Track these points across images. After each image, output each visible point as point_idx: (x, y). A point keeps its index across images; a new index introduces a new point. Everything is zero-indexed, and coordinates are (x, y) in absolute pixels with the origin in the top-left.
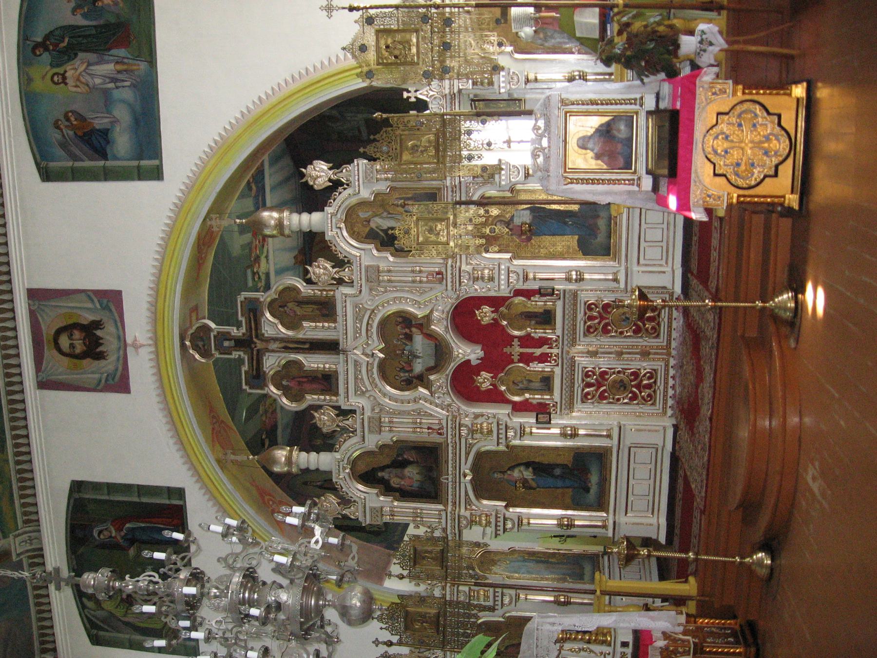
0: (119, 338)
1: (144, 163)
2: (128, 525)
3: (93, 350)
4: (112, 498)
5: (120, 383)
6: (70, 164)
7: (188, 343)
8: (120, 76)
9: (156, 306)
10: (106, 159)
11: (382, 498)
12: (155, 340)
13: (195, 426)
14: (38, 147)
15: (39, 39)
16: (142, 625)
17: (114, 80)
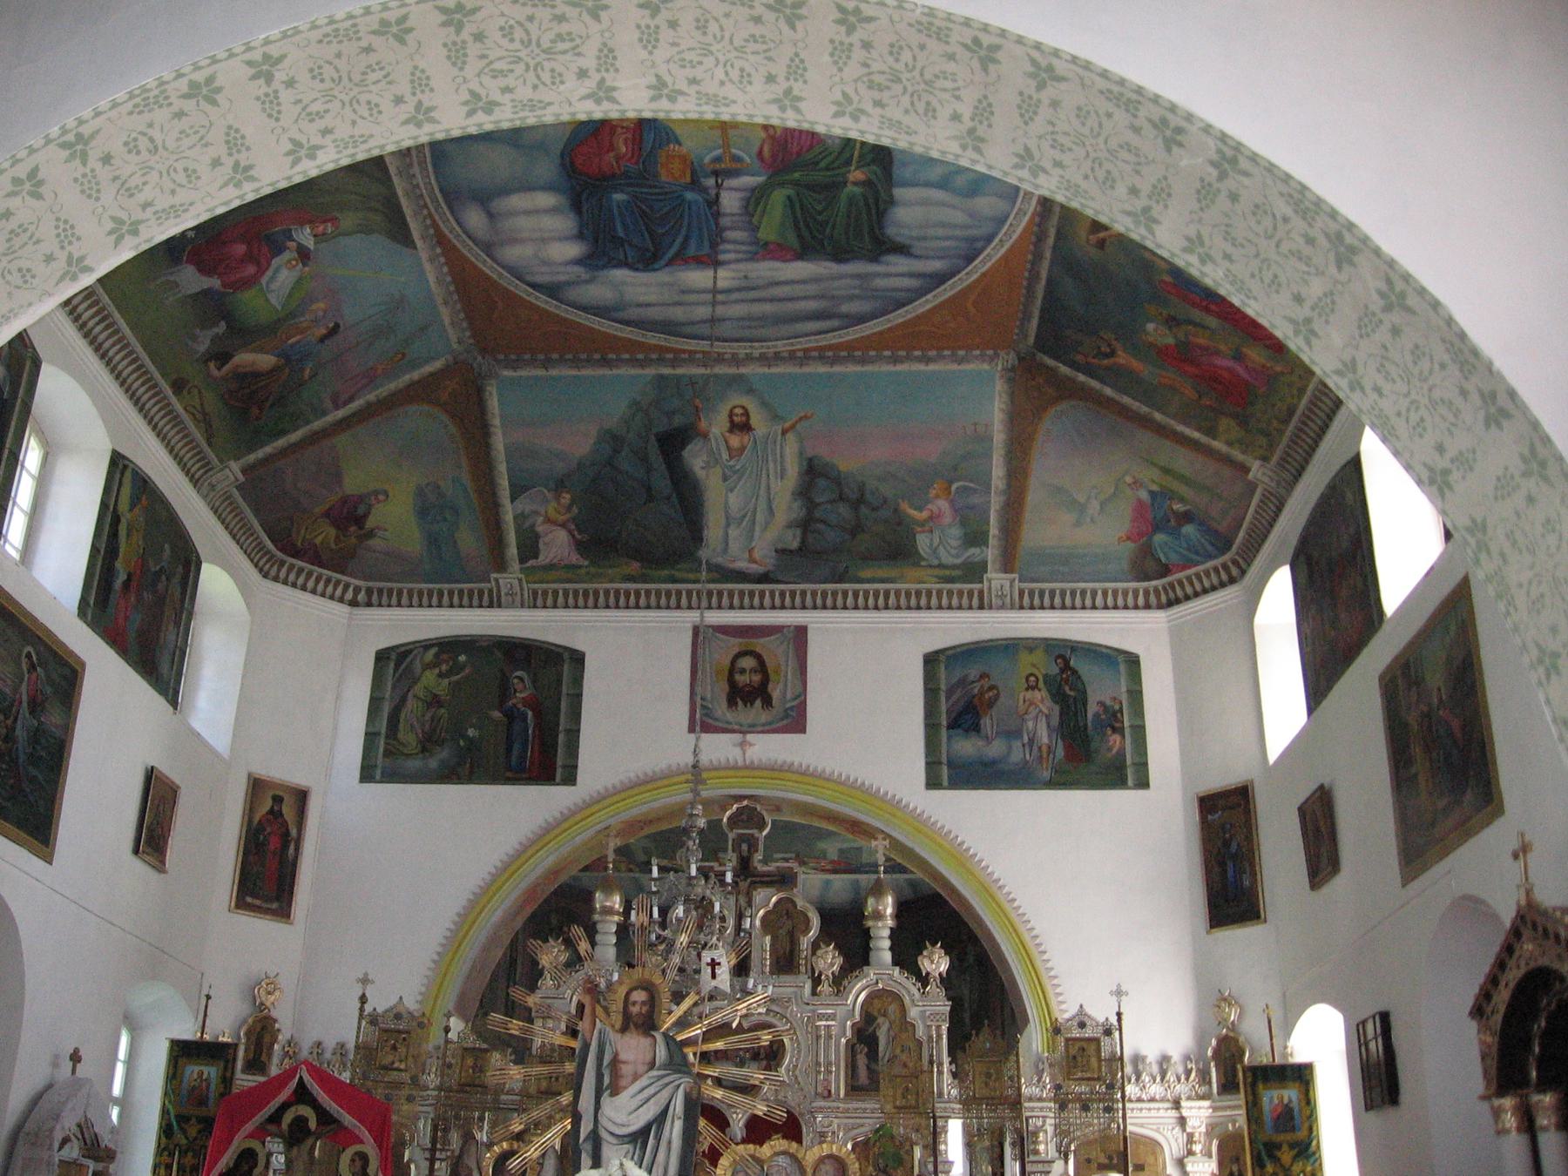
0: (753, 726)
2: (530, 713)
5: (702, 722)
6: (943, 687)
7: (745, 803)
8: (1035, 748)
12: (751, 767)
16: (403, 716)
17: (1031, 741)
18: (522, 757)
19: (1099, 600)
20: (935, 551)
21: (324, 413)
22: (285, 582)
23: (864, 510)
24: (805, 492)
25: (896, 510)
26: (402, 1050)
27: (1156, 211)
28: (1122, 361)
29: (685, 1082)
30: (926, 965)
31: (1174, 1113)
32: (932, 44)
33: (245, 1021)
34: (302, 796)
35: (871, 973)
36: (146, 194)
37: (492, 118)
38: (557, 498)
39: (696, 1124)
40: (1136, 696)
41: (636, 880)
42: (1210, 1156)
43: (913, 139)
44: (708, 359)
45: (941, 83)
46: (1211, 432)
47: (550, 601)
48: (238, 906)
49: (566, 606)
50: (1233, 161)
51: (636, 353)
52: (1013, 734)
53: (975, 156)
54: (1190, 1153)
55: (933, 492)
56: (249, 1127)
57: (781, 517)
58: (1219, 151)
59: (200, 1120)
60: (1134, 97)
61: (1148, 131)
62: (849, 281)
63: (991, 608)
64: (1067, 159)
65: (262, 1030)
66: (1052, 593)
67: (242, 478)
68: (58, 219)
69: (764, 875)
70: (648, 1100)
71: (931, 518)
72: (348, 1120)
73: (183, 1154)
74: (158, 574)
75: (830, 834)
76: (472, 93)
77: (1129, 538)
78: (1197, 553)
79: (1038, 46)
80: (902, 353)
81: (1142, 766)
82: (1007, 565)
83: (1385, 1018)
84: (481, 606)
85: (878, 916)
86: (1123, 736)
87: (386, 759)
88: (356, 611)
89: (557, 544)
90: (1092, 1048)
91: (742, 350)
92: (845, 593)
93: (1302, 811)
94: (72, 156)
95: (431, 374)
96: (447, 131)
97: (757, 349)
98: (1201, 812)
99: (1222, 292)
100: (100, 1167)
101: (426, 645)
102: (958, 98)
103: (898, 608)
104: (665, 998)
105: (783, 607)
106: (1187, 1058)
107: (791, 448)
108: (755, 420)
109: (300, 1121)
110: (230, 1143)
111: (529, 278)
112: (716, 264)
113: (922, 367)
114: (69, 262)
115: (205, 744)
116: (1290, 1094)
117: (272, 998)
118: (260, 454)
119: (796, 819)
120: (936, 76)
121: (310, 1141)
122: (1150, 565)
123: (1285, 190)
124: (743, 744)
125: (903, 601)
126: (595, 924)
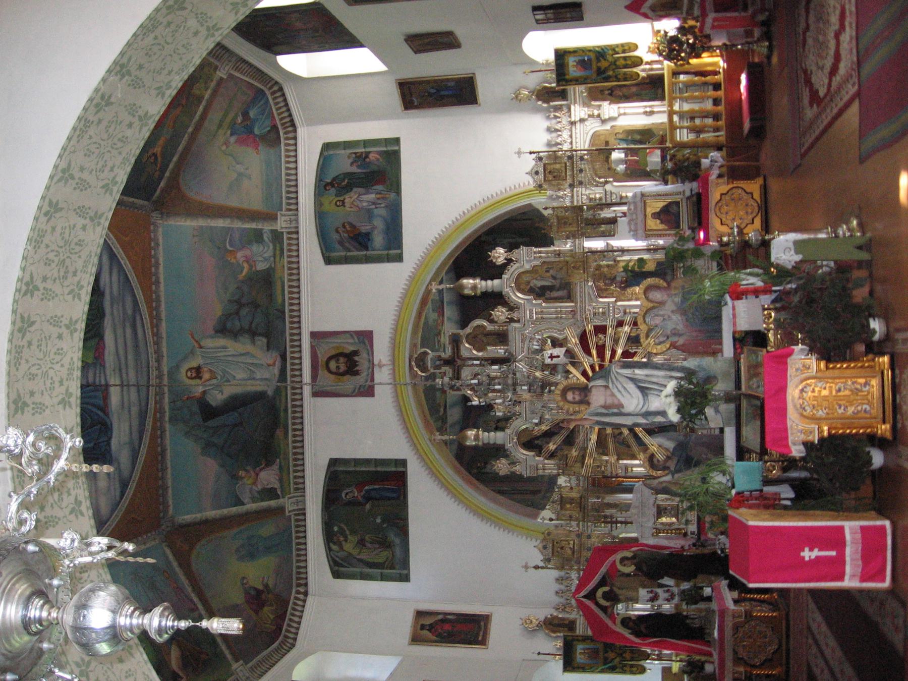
1: (392, 252)
2: (367, 488)
3: (352, 369)
4: (358, 469)
5: (369, 392)
6: (343, 254)
7: (413, 363)
8: (379, 201)
11: (537, 458)
13: (417, 416)
14: (324, 244)
15: (329, 181)
17: (374, 203)
18: (393, 490)
19: (292, 165)
20: (266, 259)
22: (297, 634)
23: (244, 301)
24: (235, 335)
26: (563, 543)
27: (141, 113)
28: (160, 149)
29: (615, 369)
30: (500, 261)
31: (578, 125)
32: (46, 240)
34: (420, 614)
35: (507, 291)
37: (83, 501)
38: (242, 478)
40: (347, 145)
41: (451, 426)
42: (600, 106)
44: (160, 394)
45: (66, 236)
46: (200, 99)
47: (300, 480)
48: (485, 644)
49: (303, 471)
50: (122, 66)
51: (158, 435)
52: (369, 214)
54: (599, 116)
55: (233, 261)
57: (249, 348)
58: (116, 75)
60: (83, 122)
61: (101, 115)
63: (297, 227)
65: (552, 625)
67: (241, 662)
69: (454, 353)
70: (625, 388)
71: (248, 262)
72: (603, 570)
73: (625, 659)
75: (426, 318)
76: (71, 513)
78: (264, 110)
79: (51, 178)
82: (273, 218)
83: (535, 9)
84: (305, 520)
85: (474, 287)
86: (370, 152)
87: (396, 568)
88: (310, 591)
89: (268, 477)
90: (549, 168)
91: (154, 374)
92: (291, 311)
93: (417, 52)
95: (174, 555)
96: (92, 527)
97: (153, 363)
99: (186, 77)
101: (329, 550)
102: (74, 226)
103: (299, 280)
105: (300, 346)
106: (548, 118)
107: (209, 343)
108: (194, 364)
109: (606, 596)
110: (619, 633)
111: (118, 498)
112: (107, 386)
115: (396, 670)
116: (571, 61)
118: (227, 652)
119: (420, 335)
120: (63, 238)
121: (615, 589)
122: (273, 136)
123: (141, 37)
124: (380, 366)
125: (294, 277)
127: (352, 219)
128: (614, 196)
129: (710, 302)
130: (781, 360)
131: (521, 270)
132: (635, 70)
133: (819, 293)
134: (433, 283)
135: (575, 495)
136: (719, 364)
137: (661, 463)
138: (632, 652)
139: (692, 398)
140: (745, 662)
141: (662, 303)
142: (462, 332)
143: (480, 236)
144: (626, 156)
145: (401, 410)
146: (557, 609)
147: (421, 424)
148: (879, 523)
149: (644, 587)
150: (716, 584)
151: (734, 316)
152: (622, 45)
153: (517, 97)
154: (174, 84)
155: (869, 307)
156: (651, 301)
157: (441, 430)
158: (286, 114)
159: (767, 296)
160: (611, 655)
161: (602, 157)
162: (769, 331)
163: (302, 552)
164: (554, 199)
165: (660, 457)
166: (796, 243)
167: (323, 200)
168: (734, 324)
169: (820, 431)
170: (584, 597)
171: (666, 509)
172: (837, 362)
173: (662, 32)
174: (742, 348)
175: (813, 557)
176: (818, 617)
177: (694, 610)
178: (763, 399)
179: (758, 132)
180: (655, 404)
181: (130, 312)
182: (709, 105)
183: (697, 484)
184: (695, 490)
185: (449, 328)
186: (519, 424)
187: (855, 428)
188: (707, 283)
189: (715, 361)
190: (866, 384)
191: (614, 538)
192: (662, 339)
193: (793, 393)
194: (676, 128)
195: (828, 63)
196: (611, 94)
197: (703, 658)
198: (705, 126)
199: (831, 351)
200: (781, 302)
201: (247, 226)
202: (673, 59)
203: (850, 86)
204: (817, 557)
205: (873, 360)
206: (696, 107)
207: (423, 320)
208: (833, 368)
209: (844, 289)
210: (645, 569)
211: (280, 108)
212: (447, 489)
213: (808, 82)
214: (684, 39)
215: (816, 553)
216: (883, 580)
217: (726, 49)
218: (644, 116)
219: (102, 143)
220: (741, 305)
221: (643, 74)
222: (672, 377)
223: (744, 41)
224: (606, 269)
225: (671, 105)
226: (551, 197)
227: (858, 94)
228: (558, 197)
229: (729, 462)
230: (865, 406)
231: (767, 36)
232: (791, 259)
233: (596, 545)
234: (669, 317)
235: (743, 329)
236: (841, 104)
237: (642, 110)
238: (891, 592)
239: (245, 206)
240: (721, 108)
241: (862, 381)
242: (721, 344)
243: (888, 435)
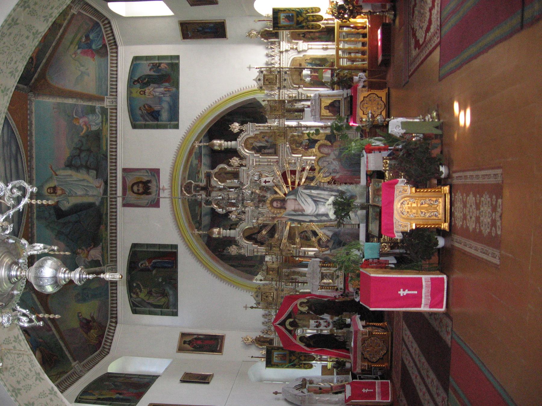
0: (157, 186)
3: (146, 191)
4: (148, 250)
5: (156, 204)
6: (144, 123)
7: (183, 189)
9: (172, 174)
10: (158, 121)
11: (254, 246)
12: (171, 187)
15: (136, 79)
16: (155, 303)
17: (163, 94)
18: (169, 263)
19: (115, 69)
20: (97, 124)
21: (54, 334)
22: (110, 346)
23: (83, 148)
24: (77, 168)
25: (83, 137)
29: (301, 190)
30: (236, 131)
31: (284, 53)
33: (257, 347)
34: (183, 335)
36: (27, 370)
39: (313, 186)
40: (148, 58)
43: (3, 112)
47: (114, 256)
48: (221, 352)
49: (116, 250)
53: (10, 91)
54: (296, 49)
55: (77, 124)
56: (293, 340)
57: (86, 177)
59: (290, 356)
62: (5, 151)
63: (116, 106)
64: (15, 59)
65: (260, 341)
66: (111, 85)
68: (39, 397)
69: (207, 181)
70: (306, 201)
72: (290, 309)
74: (115, 385)
75: (191, 162)
77: (93, 57)
78: (99, 35)
80: (29, 133)
81: (172, 57)
82: (102, 100)
85: (220, 145)
86: (161, 63)
87: (170, 308)
88: (119, 321)
94: (19, 393)
95: (38, 299)
98: (187, 39)
100: (308, 383)
101: (130, 297)
104: (276, 196)
105: (116, 176)
106: (267, 48)
109: (291, 324)
110: (298, 345)
113: (34, 126)
114: (51, 394)
116: (282, 16)
117: (250, 339)
118: (69, 355)
121: (297, 320)
126: (223, 237)
127: (150, 103)
128: (303, 96)
129: (354, 155)
130: (391, 186)
131: (248, 136)
132: (318, 23)
133: (413, 151)
134: (196, 142)
135: (275, 266)
136: (358, 188)
137: (325, 244)
138: (305, 356)
139: (343, 207)
140: (368, 360)
141: (328, 154)
142: (212, 171)
143: (224, 116)
144: (311, 73)
145: (175, 216)
146: (263, 333)
147: (186, 225)
148: (440, 276)
149: (312, 319)
150: (353, 317)
151: (367, 162)
152: (312, 8)
153: (249, 35)
154: (54, 15)
155: (440, 159)
156: (322, 153)
157: (199, 229)
158: (111, 38)
159: (386, 152)
160: (293, 358)
161: (297, 73)
162: (386, 171)
163: (114, 298)
164: (269, 96)
165: (324, 239)
166: (402, 123)
167: (132, 90)
168: (367, 167)
169: (411, 226)
170: (279, 324)
171: (326, 275)
172: (421, 188)
173: (335, 2)
174: (371, 180)
175: (405, 294)
176: (408, 333)
177: (340, 333)
178: (381, 207)
179: (386, 63)
180: (322, 210)
181: (14, 152)
182: (359, 46)
183: (344, 255)
184: (343, 259)
185: (204, 170)
186: (245, 226)
187: (430, 225)
188: (353, 144)
189: (356, 187)
190: (436, 201)
191: (297, 291)
192: (327, 174)
193: (397, 205)
194: (340, 58)
195: (425, 25)
196: (304, 37)
197: (345, 360)
198: (356, 58)
199: (419, 182)
200: (392, 156)
201: (86, 104)
202: (340, 18)
203: (436, 38)
204: (407, 294)
205: (441, 188)
206: (352, 47)
207: (189, 163)
208: (419, 192)
209: (427, 148)
210: (314, 309)
211: (109, 34)
212: (201, 262)
213: (414, 35)
214: (347, 7)
215: (407, 292)
216: (442, 307)
217: (371, 14)
218: (322, 51)
219: (11, 47)
220: (371, 156)
221: (323, 26)
222: (332, 195)
223: (380, 10)
224: (297, 138)
225: (338, 45)
226: (267, 95)
227: (440, 43)
228: (271, 95)
229: (361, 243)
230: (435, 213)
231: (394, 8)
232: (399, 132)
233: (286, 295)
234: (332, 162)
235: (372, 169)
236: (431, 48)
237: (321, 47)
238: (447, 314)
239: (85, 92)
240: (366, 48)
241: (434, 199)
242: (360, 178)
243: (447, 229)
